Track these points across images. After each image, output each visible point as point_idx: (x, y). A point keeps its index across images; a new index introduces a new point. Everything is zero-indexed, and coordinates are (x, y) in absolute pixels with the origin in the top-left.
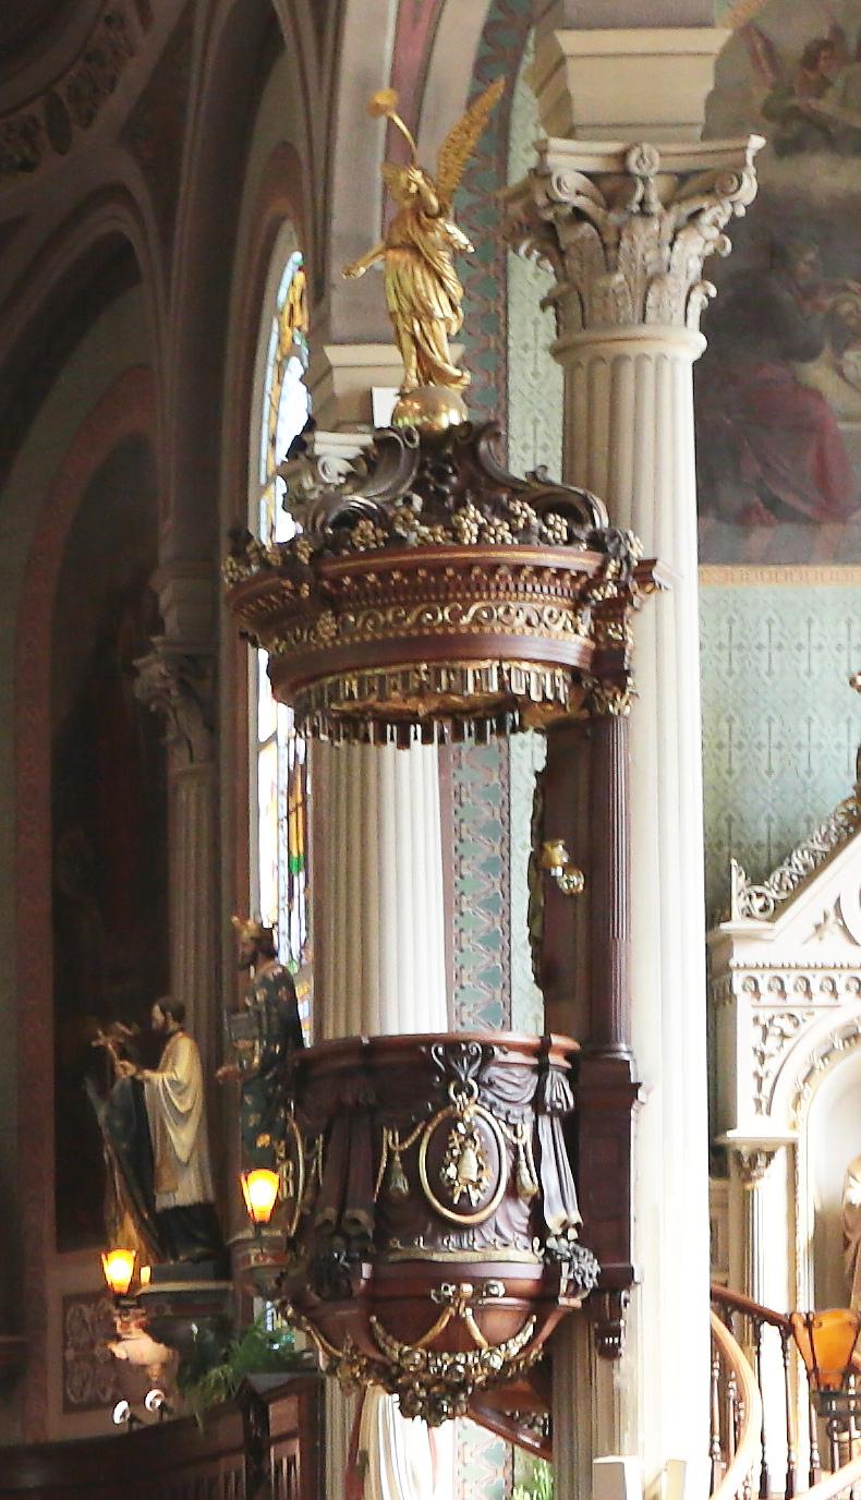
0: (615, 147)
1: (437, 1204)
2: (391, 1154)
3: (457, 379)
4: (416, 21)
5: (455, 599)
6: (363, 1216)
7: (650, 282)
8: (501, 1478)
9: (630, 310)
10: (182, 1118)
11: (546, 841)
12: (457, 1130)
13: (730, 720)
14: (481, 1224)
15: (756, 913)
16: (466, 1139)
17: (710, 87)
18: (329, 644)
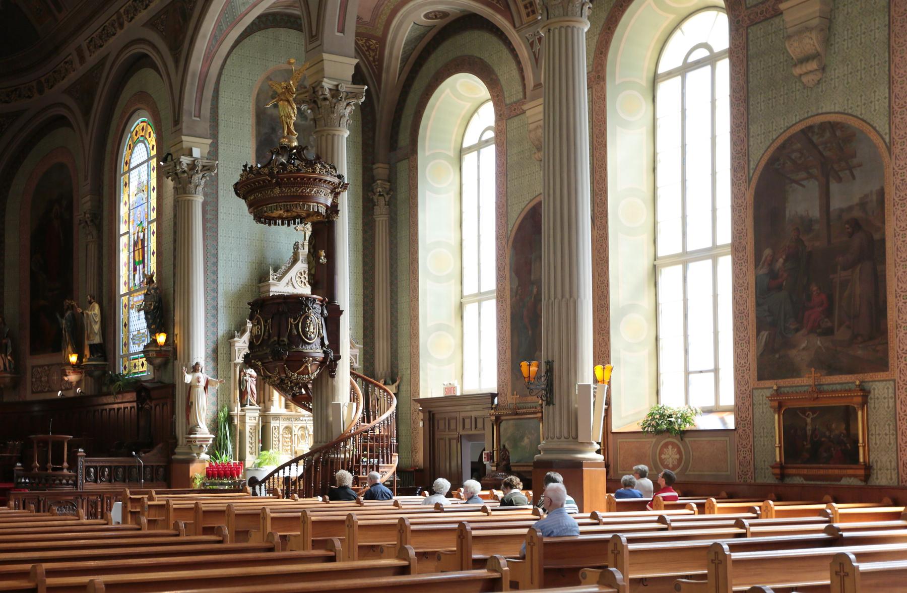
0: (336, 83)
2: (291, 324)
4: (206, 62)
6: (285, 339)
7: (341, 117)
10: (96, 322)
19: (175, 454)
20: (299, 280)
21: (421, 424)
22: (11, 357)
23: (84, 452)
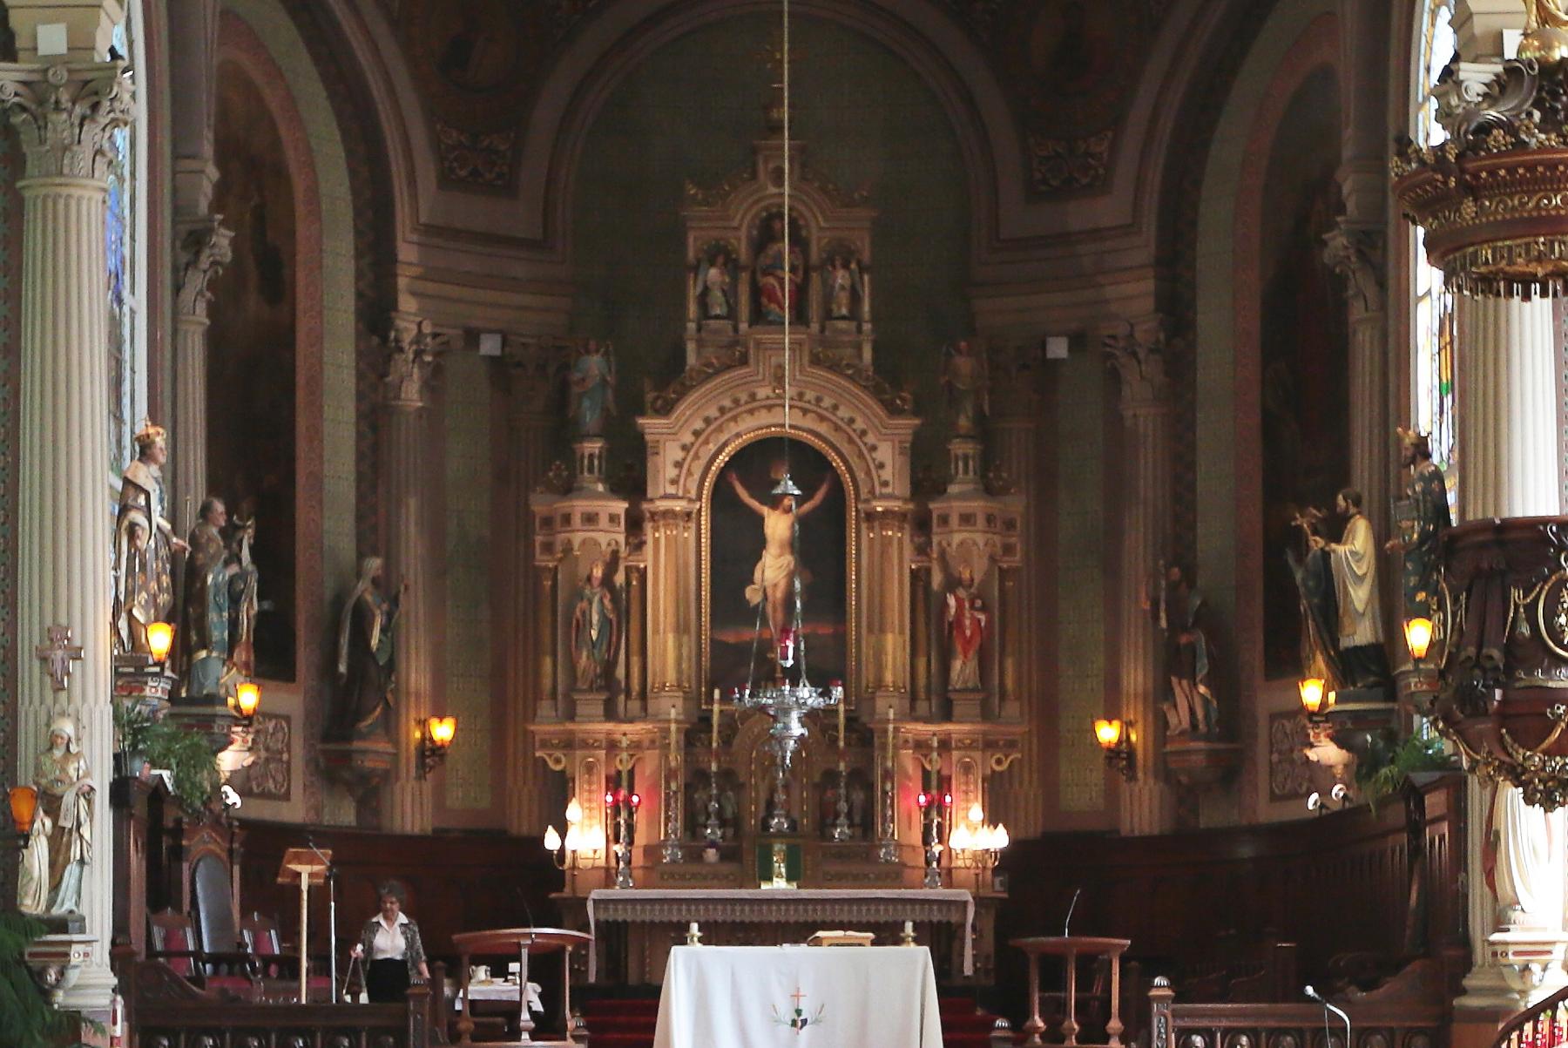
1: (1551, 644)
2: (1517, 607)
6: (1496, 653)
10: (1360, 579)
18: (1470, 223)
19: (1463, 992)
22: (1207, 686)
23: (1169, 987)
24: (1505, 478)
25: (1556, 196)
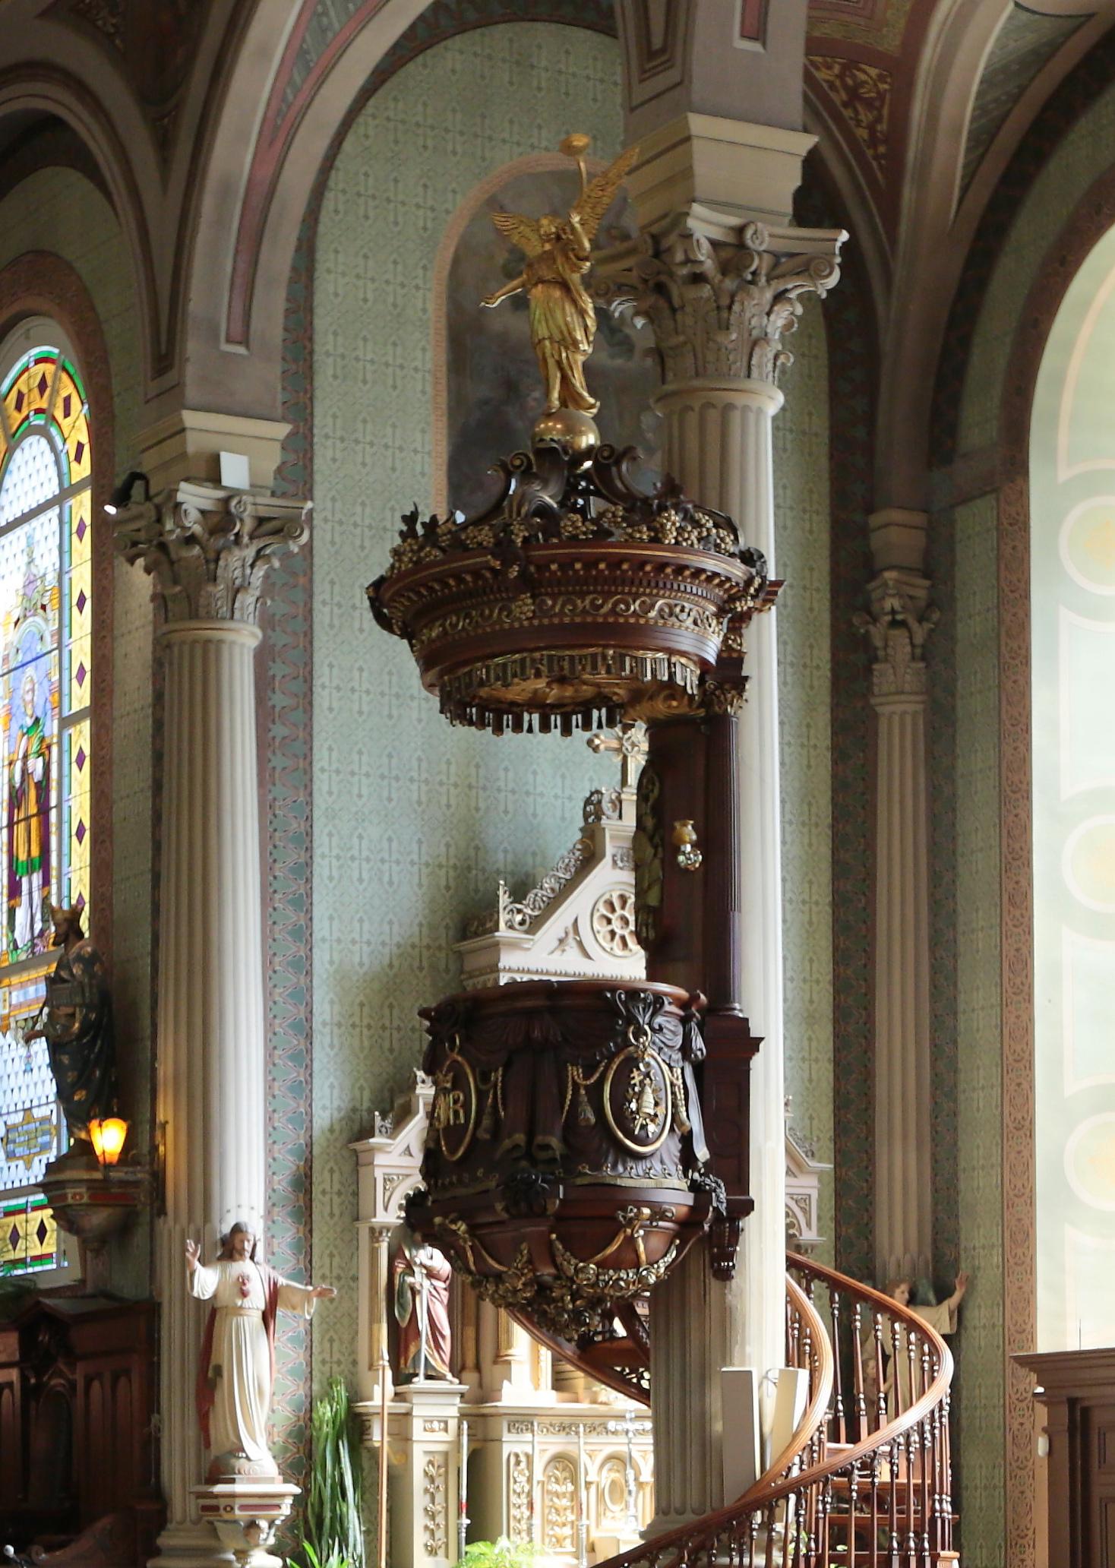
0: (734, 221)
2: (576, 1087)
3: (592, 406)
4: (271, 143)
5: (644, 594)
6: (555, 1142)
8: (301, 1392)
9: (740, 365)
11: (675, 820)
12: (638, 1069)
13: (477, 766)
14: (652, 1155)
15: (517, 926)
16: (645, 1078)
17: (799, 183)
18: (526, 623)
20: (603, 929)
21: (1042, 1445)
24: (215, 962)
25: (634, 602)
